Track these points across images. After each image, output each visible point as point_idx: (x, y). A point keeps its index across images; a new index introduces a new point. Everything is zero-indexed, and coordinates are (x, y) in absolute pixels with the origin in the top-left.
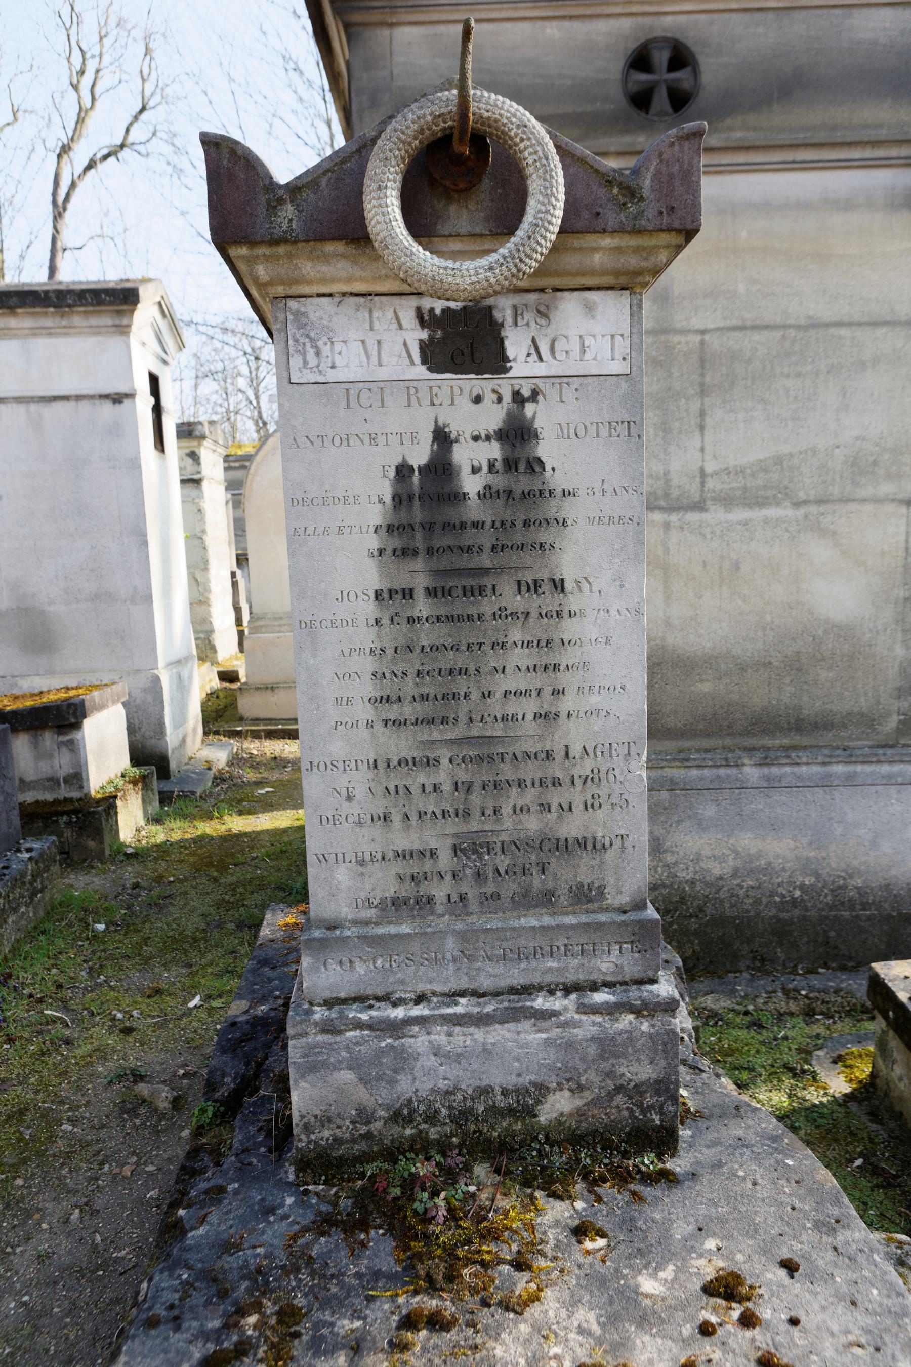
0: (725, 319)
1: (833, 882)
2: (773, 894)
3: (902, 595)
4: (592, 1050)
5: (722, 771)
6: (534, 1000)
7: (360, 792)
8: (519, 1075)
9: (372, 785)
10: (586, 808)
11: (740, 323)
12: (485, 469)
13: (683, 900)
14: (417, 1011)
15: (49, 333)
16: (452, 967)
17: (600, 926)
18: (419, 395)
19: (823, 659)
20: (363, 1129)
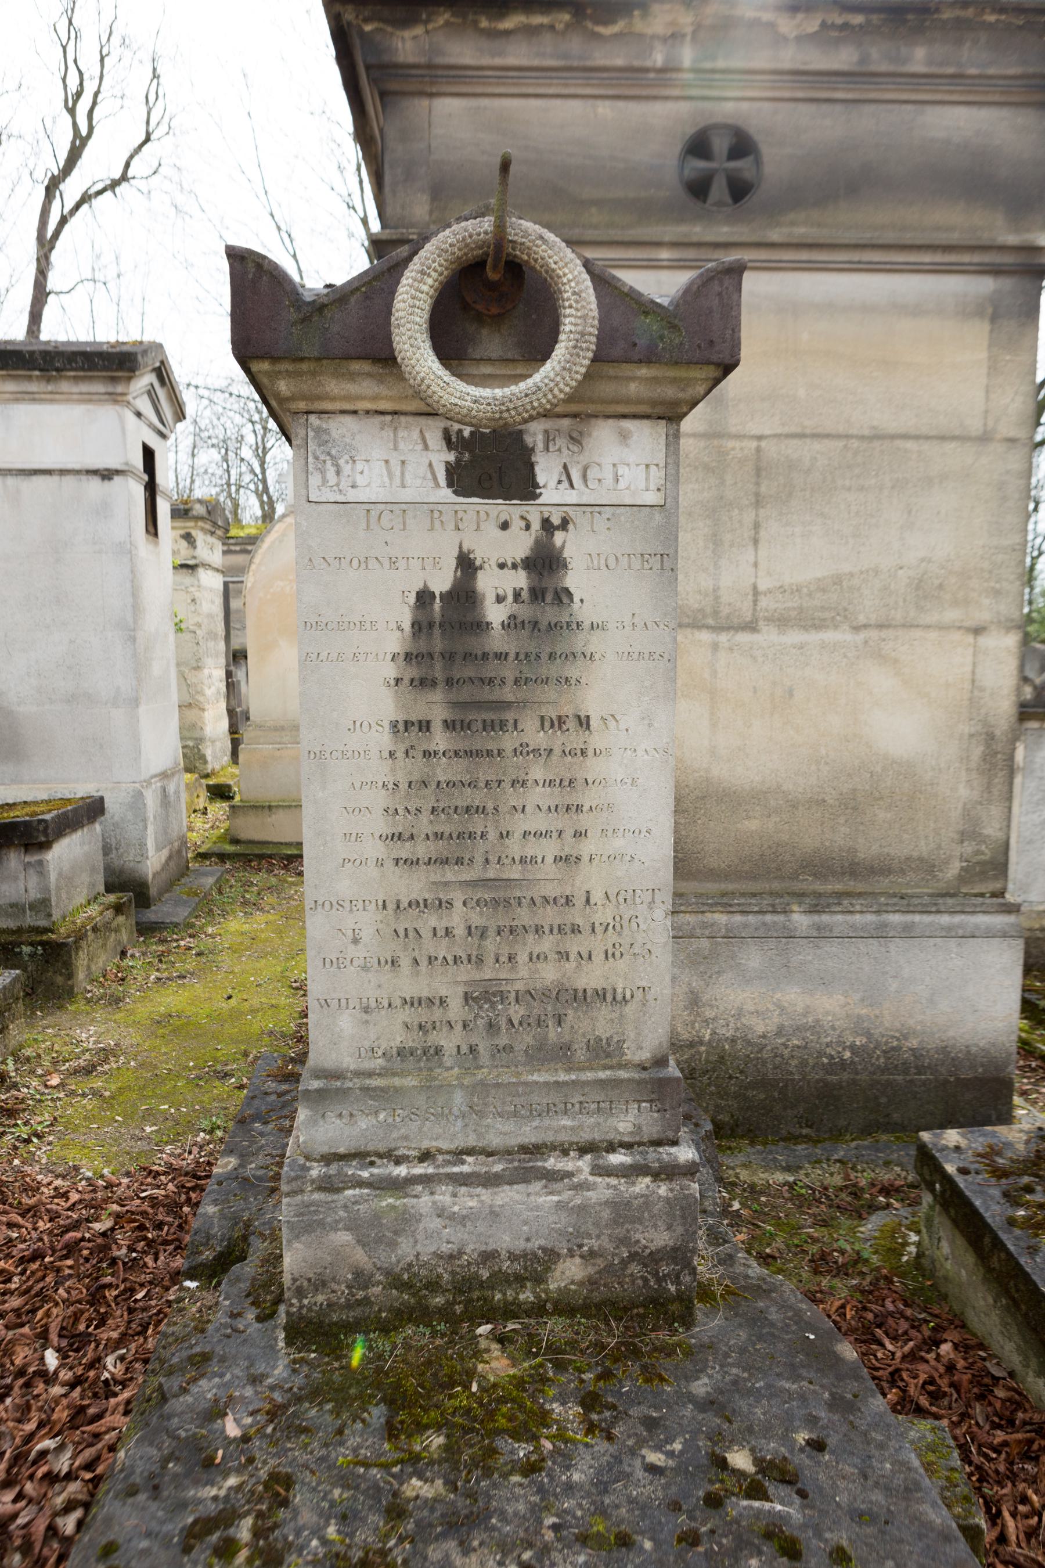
0: (783, 425)
1: (886, 1043)
2: (821, 1054)
3: (966, 731)
4: (606, 1214)
5: (769, 918)
6: (546, 1160)
7: (367, 934)
8: (528, 1240)
9: (380, 926)
10: (607, 957)
11: (799, 430)
12: (510, 598)
13: (722, 1059)
14: (419, 1170)
15: (33, 398)
16: (459, 1123)
17: (617, 1083)
18: (443, 518)
19: (882, 798)
20: (360, 1295)
